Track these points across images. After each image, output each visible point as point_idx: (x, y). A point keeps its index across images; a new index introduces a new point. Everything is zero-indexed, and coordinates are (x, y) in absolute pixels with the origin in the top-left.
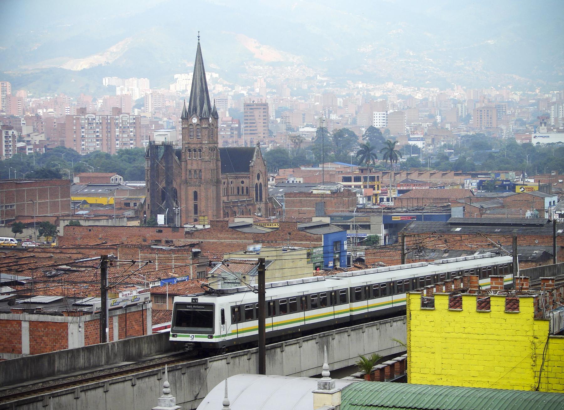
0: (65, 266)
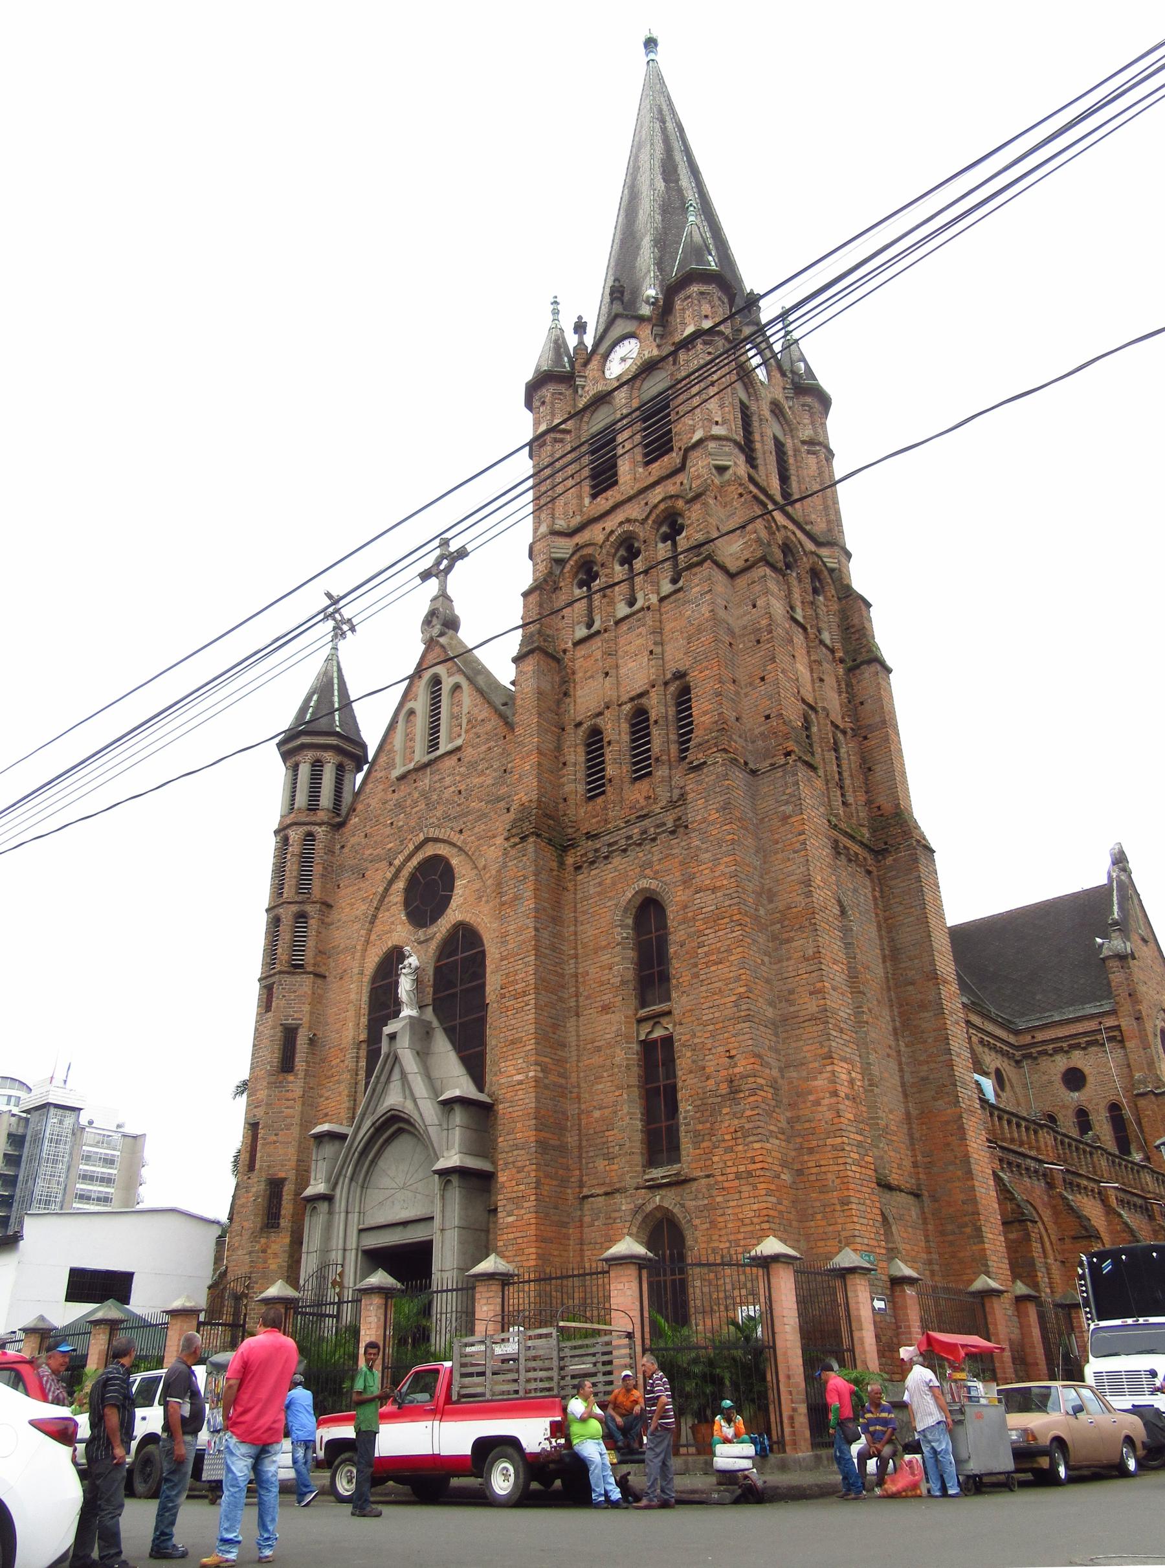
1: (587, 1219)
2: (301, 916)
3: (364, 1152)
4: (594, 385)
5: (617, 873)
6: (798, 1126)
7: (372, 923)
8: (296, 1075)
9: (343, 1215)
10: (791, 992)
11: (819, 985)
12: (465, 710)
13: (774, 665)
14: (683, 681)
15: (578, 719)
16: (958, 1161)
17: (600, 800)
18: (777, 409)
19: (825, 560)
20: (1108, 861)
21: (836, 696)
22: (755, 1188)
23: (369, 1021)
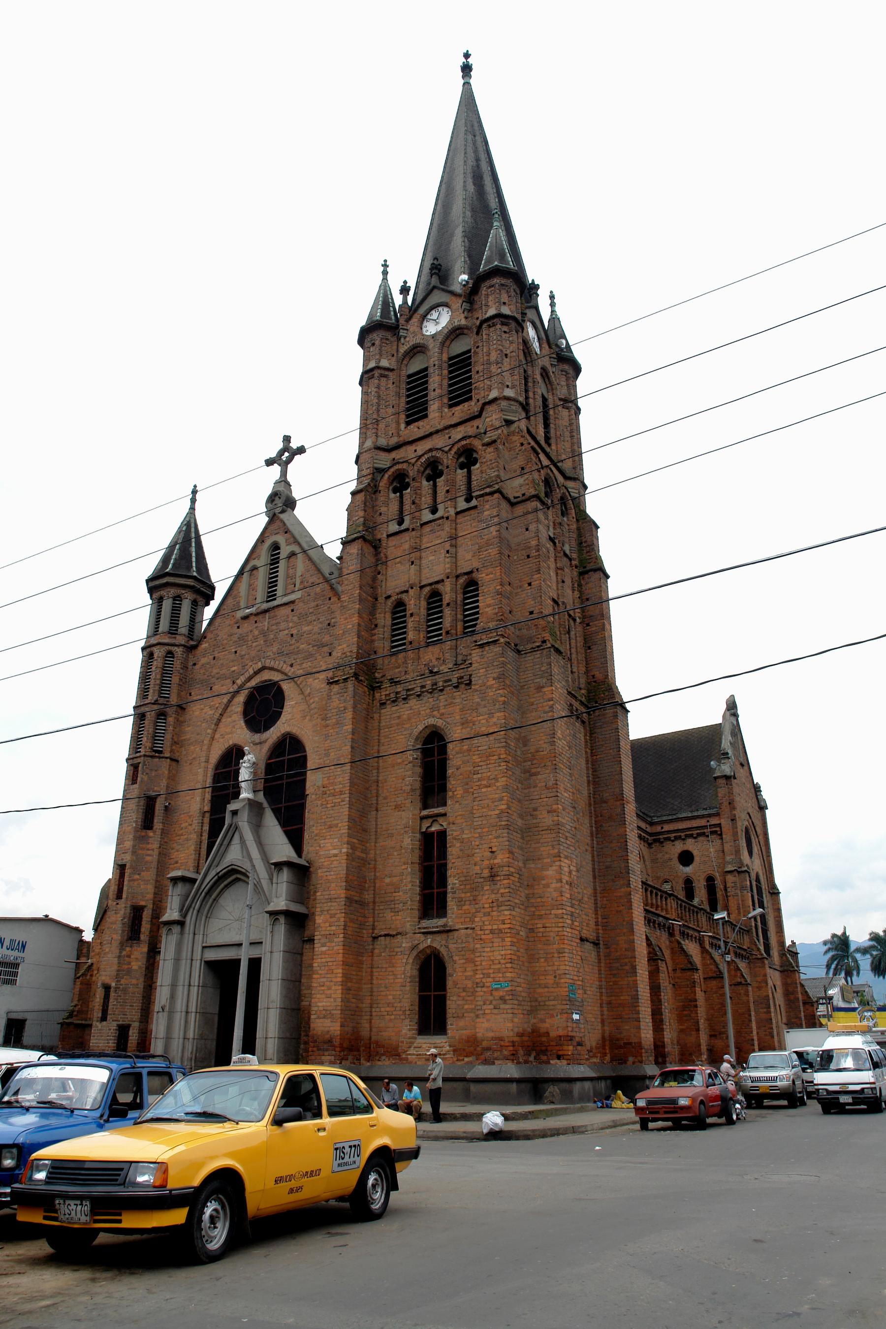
0: (716, 1118)
1: (376, 951)
2: (162, 715)
3: (209, 893)
4: (413, 337)
5: (412, 711)
6: (532, 900)
7: (217, 725)
8: (155, 832)
9: (191, 935)
10: (535, 810)
11: (555, 807)
12: (299, 574)
13: (539, 575)
14: (470, 576)
15: (389, 593)
16: (625, 923)
17: (401, 656)
18: (545, 373)
19: (570, 490)
20: (724, 707)
21: (571, 593)
22: (503, 940)
23: (212, 797)
